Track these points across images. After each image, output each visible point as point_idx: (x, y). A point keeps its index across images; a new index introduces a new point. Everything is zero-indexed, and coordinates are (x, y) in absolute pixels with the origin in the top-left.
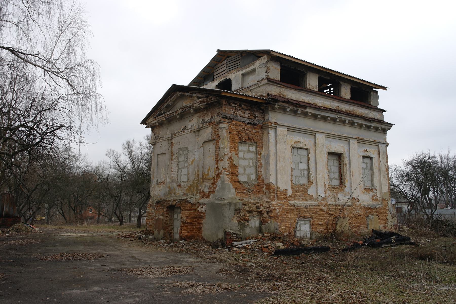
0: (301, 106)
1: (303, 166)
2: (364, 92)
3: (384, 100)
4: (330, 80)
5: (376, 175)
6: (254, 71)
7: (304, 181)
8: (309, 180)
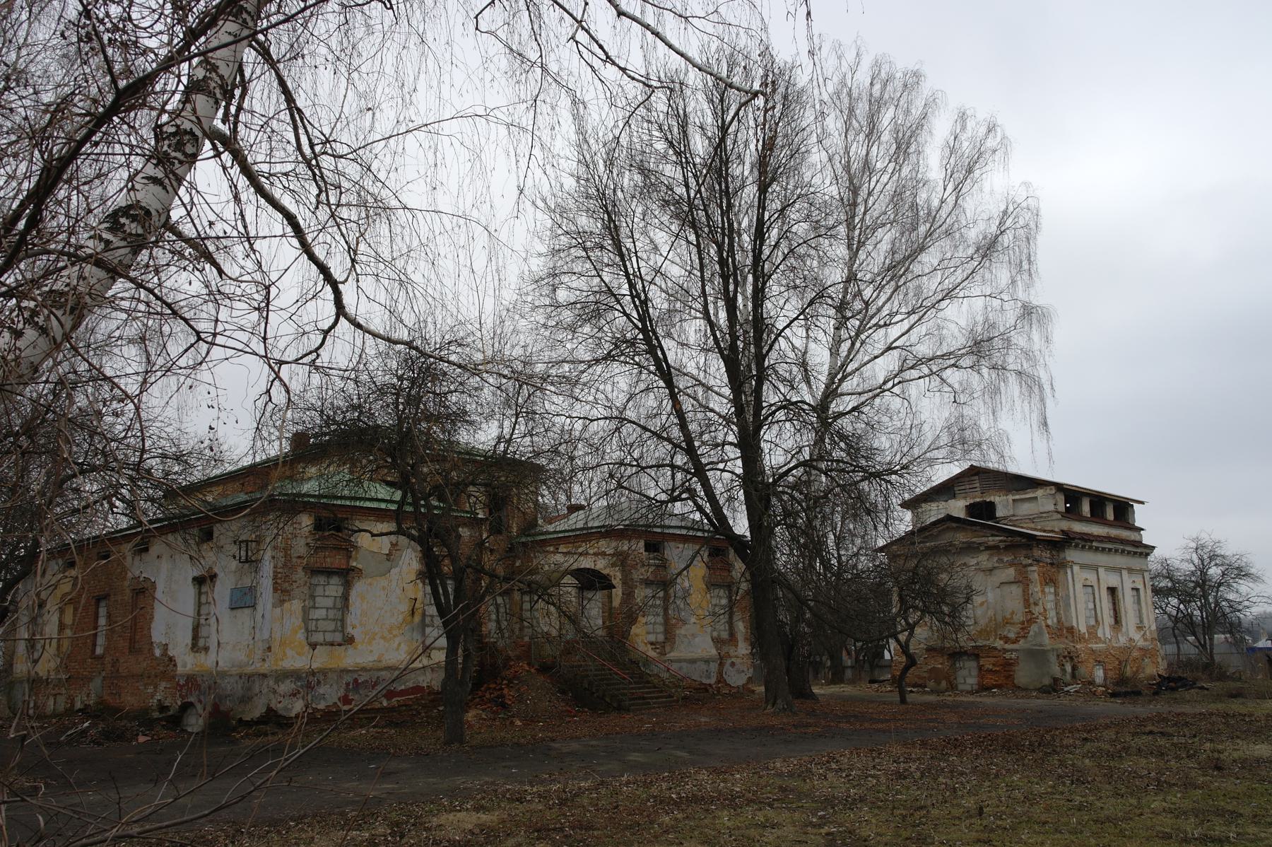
0: (1086, 541)
1: (1091, 606)
2: (1123, 508)
3: (1140, 516)
4: (1099, 501)
5: (1144, 611)
6: (1036, 498)
7: (1093, 622)
8: (1097, 621)
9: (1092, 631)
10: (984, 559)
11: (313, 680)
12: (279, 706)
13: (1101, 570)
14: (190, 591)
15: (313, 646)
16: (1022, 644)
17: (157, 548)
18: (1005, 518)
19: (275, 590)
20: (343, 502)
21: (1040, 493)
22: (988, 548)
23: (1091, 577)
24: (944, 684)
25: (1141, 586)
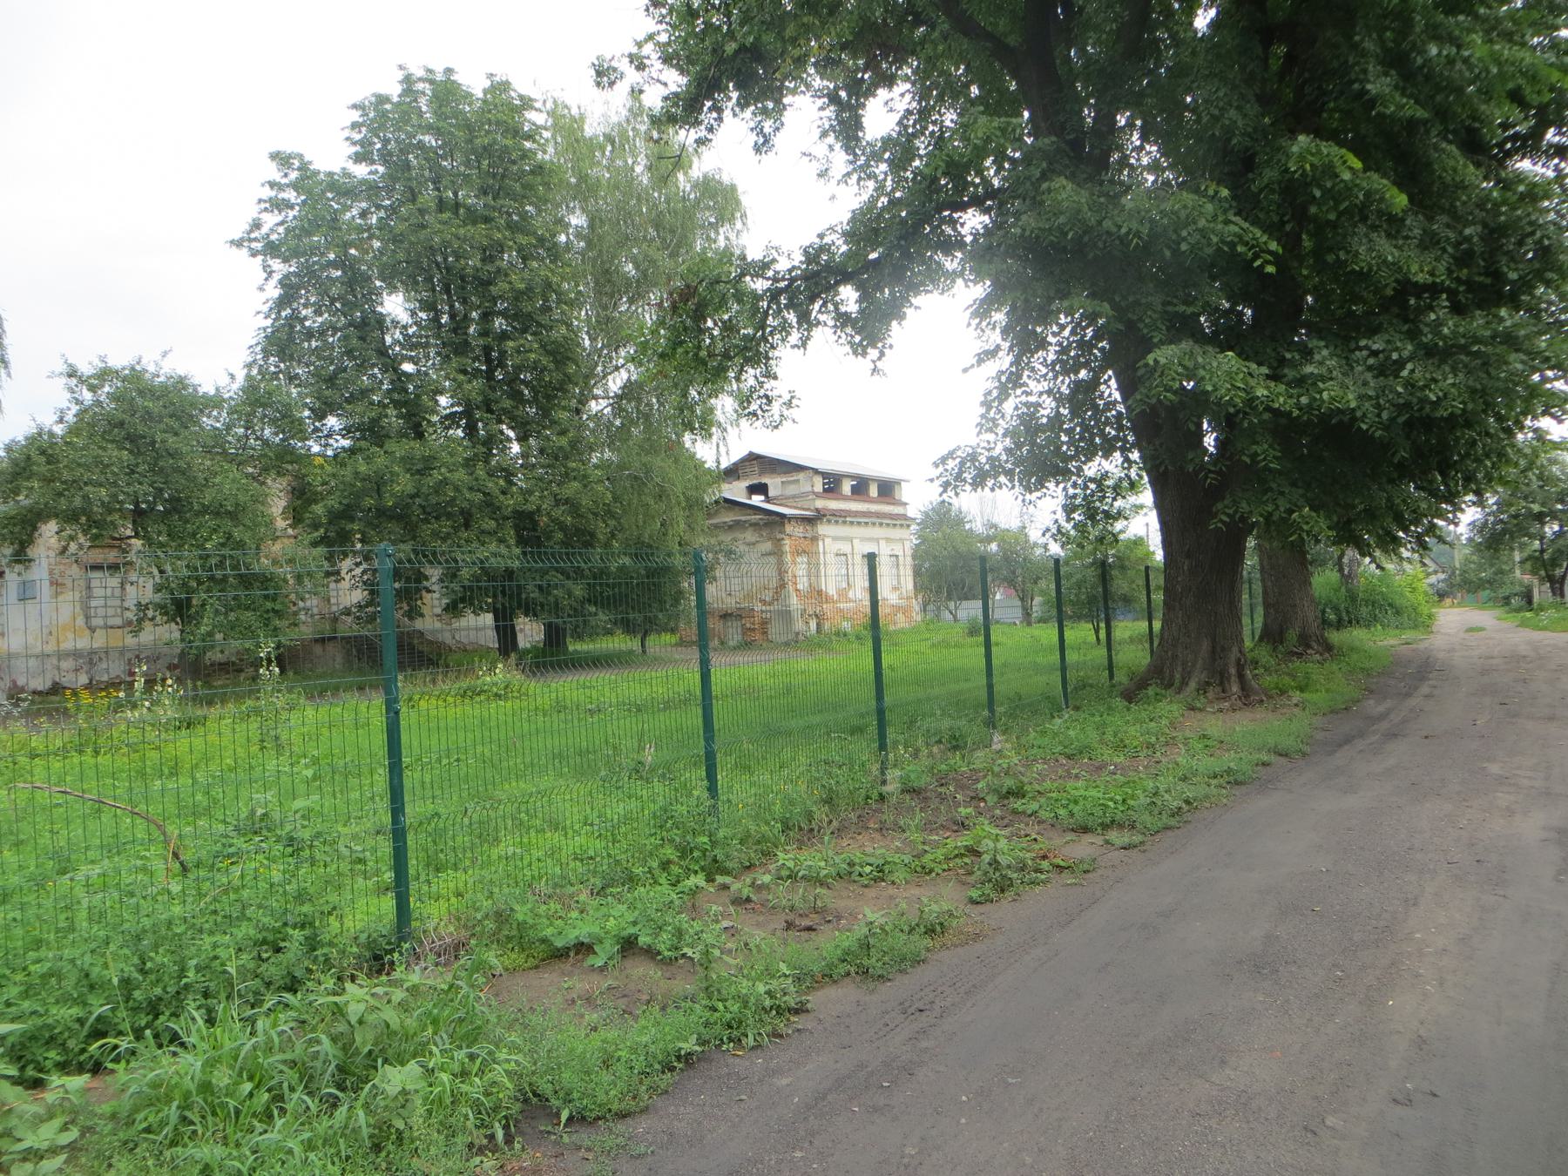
1: (844, 571)
7: (844, 585)
9: (843, 593)
10: (750, 536)
15: (92, 630)
16: (776, 607)
19: (52, 583)
21: (801, 476)
25: (900, 553)
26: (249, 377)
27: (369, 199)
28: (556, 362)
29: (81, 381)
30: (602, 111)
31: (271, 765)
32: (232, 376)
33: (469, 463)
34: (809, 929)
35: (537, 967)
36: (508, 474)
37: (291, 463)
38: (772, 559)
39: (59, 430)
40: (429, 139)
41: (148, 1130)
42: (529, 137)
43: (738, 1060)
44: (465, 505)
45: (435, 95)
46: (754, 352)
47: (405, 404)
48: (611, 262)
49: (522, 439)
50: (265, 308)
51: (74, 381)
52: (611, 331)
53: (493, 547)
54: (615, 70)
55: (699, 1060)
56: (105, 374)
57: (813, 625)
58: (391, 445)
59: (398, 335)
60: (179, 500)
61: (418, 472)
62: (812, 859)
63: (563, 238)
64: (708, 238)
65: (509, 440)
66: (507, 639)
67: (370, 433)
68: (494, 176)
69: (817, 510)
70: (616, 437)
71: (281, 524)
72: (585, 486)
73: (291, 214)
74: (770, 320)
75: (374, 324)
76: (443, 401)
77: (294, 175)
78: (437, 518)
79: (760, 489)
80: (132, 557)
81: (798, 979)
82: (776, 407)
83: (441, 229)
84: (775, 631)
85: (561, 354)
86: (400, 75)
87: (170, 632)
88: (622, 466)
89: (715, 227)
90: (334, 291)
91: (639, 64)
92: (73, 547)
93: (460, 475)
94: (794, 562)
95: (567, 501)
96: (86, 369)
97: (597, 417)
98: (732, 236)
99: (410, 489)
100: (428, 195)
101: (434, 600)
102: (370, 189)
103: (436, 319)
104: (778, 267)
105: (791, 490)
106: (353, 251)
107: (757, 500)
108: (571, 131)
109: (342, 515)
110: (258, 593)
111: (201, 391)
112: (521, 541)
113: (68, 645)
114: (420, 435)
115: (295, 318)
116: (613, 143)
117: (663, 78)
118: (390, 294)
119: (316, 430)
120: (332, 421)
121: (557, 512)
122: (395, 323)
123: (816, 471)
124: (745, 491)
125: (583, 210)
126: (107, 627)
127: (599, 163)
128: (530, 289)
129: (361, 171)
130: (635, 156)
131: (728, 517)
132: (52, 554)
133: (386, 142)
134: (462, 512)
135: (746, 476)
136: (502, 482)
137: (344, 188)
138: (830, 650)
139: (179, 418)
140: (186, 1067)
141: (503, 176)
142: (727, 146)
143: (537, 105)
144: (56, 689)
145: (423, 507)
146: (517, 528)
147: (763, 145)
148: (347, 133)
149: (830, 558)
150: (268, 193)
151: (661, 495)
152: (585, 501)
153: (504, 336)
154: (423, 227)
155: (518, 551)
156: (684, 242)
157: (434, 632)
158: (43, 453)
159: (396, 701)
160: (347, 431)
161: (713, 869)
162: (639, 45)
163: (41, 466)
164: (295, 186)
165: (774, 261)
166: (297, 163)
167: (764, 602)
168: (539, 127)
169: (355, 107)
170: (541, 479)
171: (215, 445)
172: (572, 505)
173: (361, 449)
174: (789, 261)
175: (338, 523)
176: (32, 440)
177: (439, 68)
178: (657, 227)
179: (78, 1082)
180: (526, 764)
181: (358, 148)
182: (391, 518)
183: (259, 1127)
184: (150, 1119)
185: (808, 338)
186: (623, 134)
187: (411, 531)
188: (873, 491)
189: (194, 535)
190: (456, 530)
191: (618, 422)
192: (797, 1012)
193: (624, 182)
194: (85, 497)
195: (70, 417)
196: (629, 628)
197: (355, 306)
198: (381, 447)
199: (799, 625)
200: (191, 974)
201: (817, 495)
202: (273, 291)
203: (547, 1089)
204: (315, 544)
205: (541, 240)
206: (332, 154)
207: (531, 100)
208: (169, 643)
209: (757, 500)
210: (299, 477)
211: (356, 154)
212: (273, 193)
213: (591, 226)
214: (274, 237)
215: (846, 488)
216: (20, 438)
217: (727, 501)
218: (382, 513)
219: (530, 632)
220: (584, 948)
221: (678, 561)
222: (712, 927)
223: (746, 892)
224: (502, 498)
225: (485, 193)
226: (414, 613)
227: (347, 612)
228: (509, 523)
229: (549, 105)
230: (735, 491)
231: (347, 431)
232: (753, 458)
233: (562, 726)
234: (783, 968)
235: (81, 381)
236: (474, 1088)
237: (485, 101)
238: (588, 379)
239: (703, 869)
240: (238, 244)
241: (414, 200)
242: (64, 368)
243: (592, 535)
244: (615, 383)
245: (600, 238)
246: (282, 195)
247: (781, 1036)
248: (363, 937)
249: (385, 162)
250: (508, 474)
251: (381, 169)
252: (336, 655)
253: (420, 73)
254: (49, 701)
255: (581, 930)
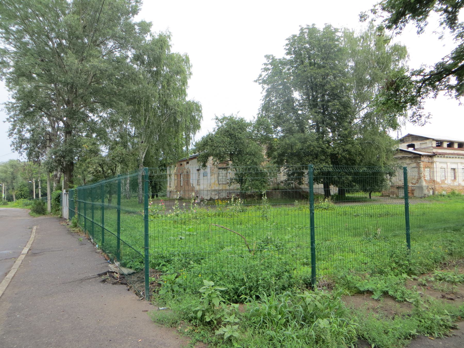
1: (443, 174)
6: (426, 143)
9: (443, 182)
10: (408, 161)
11: (220, 192)
12: (213, 197)
13: (448, 164)
14: (197, 172)
16: (417, 185)
17: (190, 162)
18: (417, 149)
20: (182, 181)
21: (427, 141)
22: (409, 158)
23: (444, 166)
24: (395, 196)
26: (258, 117)
27: (290, 65)
28: (344, 108)
29: (219, 120)
30: (359, 29)
31: (265, 224)
32: (254, 117)
33: (317, 140)
34: (452, 299)
35: (353, 295)
36: (329, 142)
37: (269, 140)
38: (416, 170)
39: (214, 133)
40: (307, 46)
41: (254, 323)
42: (337, 40)
43: (432, 341)
44: (316, 152)
45: (309, 32)
46: (413, 101)
47: (299, 123)
48: (362, 76)
49: (333, 132)
50: (262, 98)
51: (217, 120)
52: (362, 98)
53: (324, 164)
54: (366, 15)
55: (417, 337)
56: (224, 118)
57: (431, 192)
58: (295, 135)
59: (297, 103)
60: (241, 151)
61: (303, 142)
62: (450, 274)
63: (347, 70)
64: (396, 65)
65: (329, 132)
66: (327, 193)
67: (289, 131)
68: (326, 53)
69: (434, 153)
70: (363, 130)
71: (265, 157)
72: (353, 146)
73: (270, 72)
74: (422, 90)
75: (290, 101)
76: (310, 121)
77: (270, 61)
78: (308, 156)
79: (412, 146)
80: (230, 166)
81: (453, 317)
82: (423, 119)
83: (310, 71)
84: (416, 193)
85: (346, 106)
86: (299, 28)
87: (238, 186)
88: (365, 139)
89: (398, 61)
90: (280, 92)
91: (374, 12)
92: (216, 163)
93: (315, 143)
94: (424, 170)
95: (347, 151)
96: (220, 118)
97: (356, 125)
98: (404, 63)
99: (300, 147)
100: (307, 61)
101: (306, 180)
102: (291, 62)
103: (309, 98)
104: (425, 71)
105: (424, 146)
106: (285, 80)
107: (411, 149)
108: (350, 36)
109: (281, 155)
110: (260, 176)
111: (246, 122)
112: (332, 163)
113: (213, 188)
114: (303, 132)
115: (270, 100)
116: (363, 38)
117: (382, 15)
118: (296, 91)
119: (275, 131)
120: (279, 129)
121: (344, 154)
122: (297, 100)
123: (433, 140)
124: (406, 147)
125: (353, 60)
126: (222, 184)
127: (359, 45)
128: (336, 86)
129: (288, 57)
130: (370, 41)
131: (400, 155)
132: (211, 165)
133: (295, 48)
134: (315, 154)
135: (407, 141)
136: (327, 145)
137: (283, 63)
138: (438, 201)
139: (241, 129)
140: (264, 307)
141: (329, 53)
142: (408, 35)
143: (339, 30)
144: (211, 199)
145: (304, 152)
146: (331, 158)
147: (421, 31)
148: (285, 47)
149: (438, 170)
150: (264, 67)
151: (378, 148)
152: (353, 150)
153: (328, 101)
154: (305, 71)
155: (331, 165)
156: (387, 66)
157: (305, 189)
158: (210, 139)
159: (313, 210)
160: (283, 131)
161: (410, 273)
162: (375, 6)
163: (210, 143)
164: (271, 64)
165: (424, 69)
166: (271, 57)
167: (413, 183)
168: (340, 37)
169: (287, 39)
170: (338, 144)
171: (250, 136)
172: (349, 152)
173: (287, 136)
174: (430, 68)
175: (281, 156)
176: (208, 136)
177: (310, 25)
178: (378, 63)
179: (237, 306)
180: (348, 233)
181: (287, 51)
182: (295, 156)
183: (284, 329)
184: (255, 320)
185: (437, 94)
186: (367, 35)
187: (300, 159)
188: (456, 146)
189: (244, 160)
190: (313, 159)
191: (363, 126)
192: (452, 328)
193: (367, 51)
194: (220, 150)
195: (216, 130)
196: (365, 190)
197: (286, 95)
198: (292, 135)
199: (426, 192)
200: (260, 281)
201: (434, 148)
202: (265, 93)
203: (366, 336)
204: (274, 163)
205: (340, 71)
206: (281, 53)
207: (338, 29)
208: (237, 189)
209: (411, 149)
210: (270, 144)
211: (287, 53)
212: (265, 67)
213: (356, 65)
214: (265, 79)
215: (445, 145)
216: (205, 136)
217: (401, 150)
218: (292, 154)
219: (334, 190)
220: (370, 292)
221: (383, 169)
222: (414, 293)
223: (424, 282)
224: (327, 149)
225: (323, 59)
226: (300, 183)
227: (282, 182)
228: (329, 157)
229: (343, 30)
230: (403, 147)
231: (283, 131)
232: (409, 136)
233: (347, 220)
234: (446, 312)
235: (219, 120)
236: (344, 330)
237: (324, 32)
238: (353, 114)
239: (406, 272)
240: (256, 81)
241: (303, 64)
242: (215, 117)
243: (355, 161)
244: (362, 114)
245: (359, 69)
246: (268, 67)
247: (447, 336)
248: (303, 278)
249: (294, 54)
250: (329, 142)
251: (294, 56)
252: (278, 195)
253: (305, 27)
254: (211, 202)
255: (369, 287)
